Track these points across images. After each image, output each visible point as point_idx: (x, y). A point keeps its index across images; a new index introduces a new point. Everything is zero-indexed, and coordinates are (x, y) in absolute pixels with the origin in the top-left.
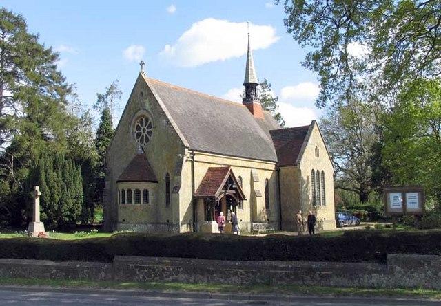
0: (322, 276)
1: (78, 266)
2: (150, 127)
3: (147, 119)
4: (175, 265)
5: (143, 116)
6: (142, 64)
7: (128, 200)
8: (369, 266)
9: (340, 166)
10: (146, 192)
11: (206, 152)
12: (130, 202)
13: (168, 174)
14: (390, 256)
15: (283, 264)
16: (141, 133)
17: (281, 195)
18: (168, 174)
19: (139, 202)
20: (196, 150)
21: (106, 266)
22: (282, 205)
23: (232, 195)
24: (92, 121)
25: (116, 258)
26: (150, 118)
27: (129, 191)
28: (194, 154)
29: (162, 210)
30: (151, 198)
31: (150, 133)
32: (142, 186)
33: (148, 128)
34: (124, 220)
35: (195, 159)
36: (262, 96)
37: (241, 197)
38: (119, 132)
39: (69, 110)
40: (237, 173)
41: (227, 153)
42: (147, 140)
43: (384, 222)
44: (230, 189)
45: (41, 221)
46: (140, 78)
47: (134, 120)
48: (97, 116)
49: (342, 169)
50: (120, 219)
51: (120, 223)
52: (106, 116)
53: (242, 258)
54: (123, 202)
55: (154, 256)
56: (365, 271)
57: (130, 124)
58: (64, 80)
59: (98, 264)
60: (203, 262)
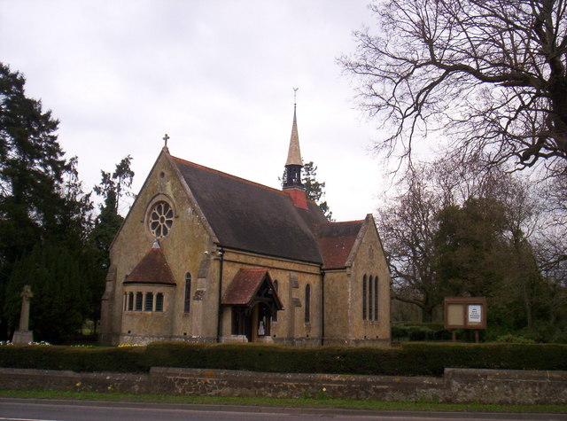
0: (377, 391)
1: (108, 378)
2: (170, 214)
3: (167, 206)
4: (219, 377)
5: (162, 202)
6: (166, 138)
7: (137, 306)
8: (427, 380)
9: (399, 269)
10: (160, 296)
11: (250, 252)
12: (139, 307)
13: (188, 275)
14: (447, 370)
15: (338, 377)
17: (325, 306)
18: (188, 275)
20: (228, 248)
21: (141, 378)
22: (326, 319)
23: (266, 303)
25: (153, 369)
26: (171, 204)
27: (140, 295)
28: (223, 252)
29: (179, 321)
31: (170, 223)
32: (155, 290)
34: (129, 332)
35: (224, 258)
36: (306, 179)
37: (279, 307)
38: (130, 220)
39: (65, 191)
40: (273, 276)
41: (286, 256)
42: (165, 232)
44: (265, 296)
45: (30, 329)
46: (165, 152)
47: (150, 206)
48: (99, 201)
49: (400, 275)
50: (125, 331)
51: (125, 335)
52: (112, 200)
53: (294, 370)
54: (131, 308)
55: (195, 367)
56: (421, 385)
58: (62, 154)
59: (130, 376)
60: (250, 374)
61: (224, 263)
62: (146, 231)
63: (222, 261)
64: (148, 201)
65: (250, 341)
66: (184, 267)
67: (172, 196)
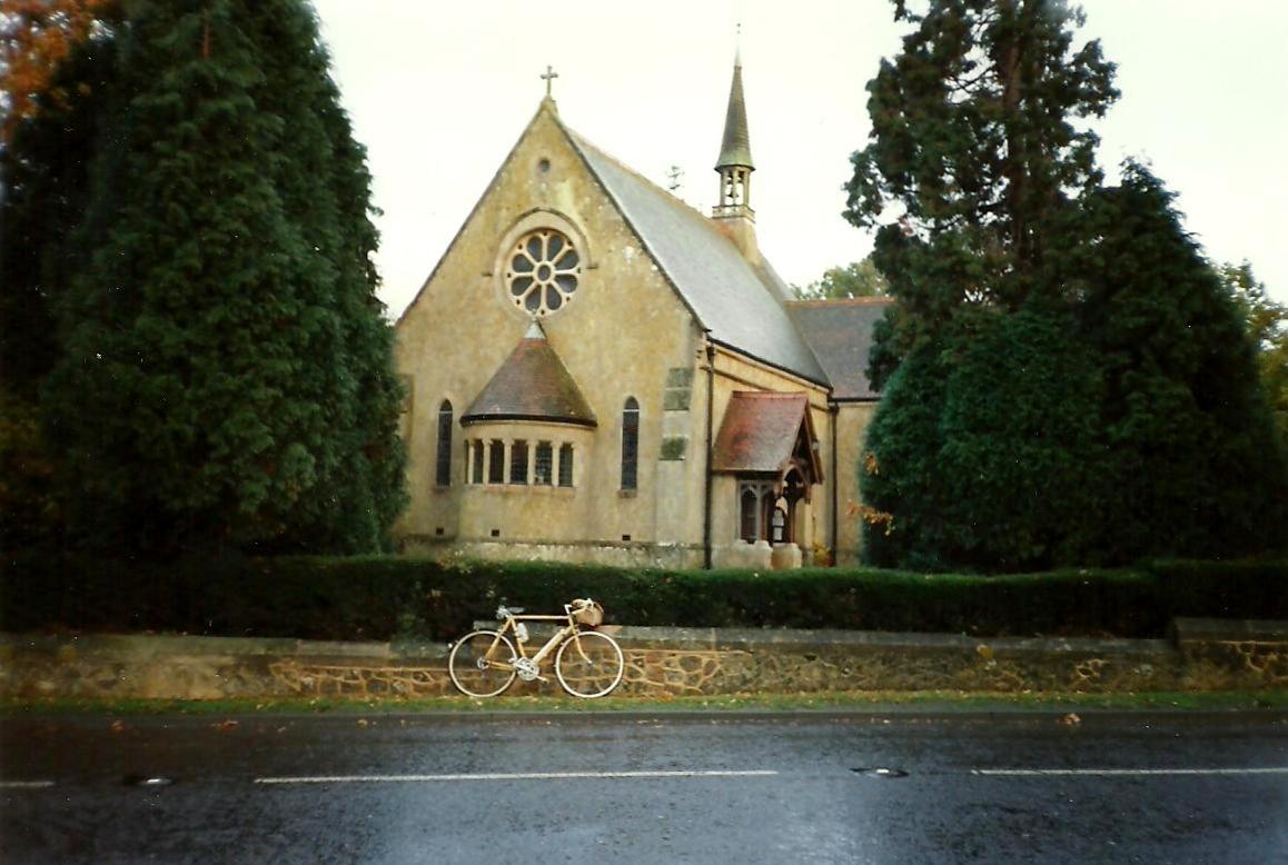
5: (545, 230)
10: (566, 450)
13: (632, 403)
16: (558, 265)
18: (446, 405)
19: (548, 481)
24: (1083, 13)
30: (579, 469)
32: (558, 435)
33: (550, 259)
34: (495, 533)
42: (554, 302)
43: (359, 666)
46: (547, 110)
54: (478, 478)
57: (494, 250)
61: (717, 379)
62: (499, 299)
63: (711, 372)
64: (503, 226)
65: (524, 644)
66: (617, 383)
67: (576, 218)
